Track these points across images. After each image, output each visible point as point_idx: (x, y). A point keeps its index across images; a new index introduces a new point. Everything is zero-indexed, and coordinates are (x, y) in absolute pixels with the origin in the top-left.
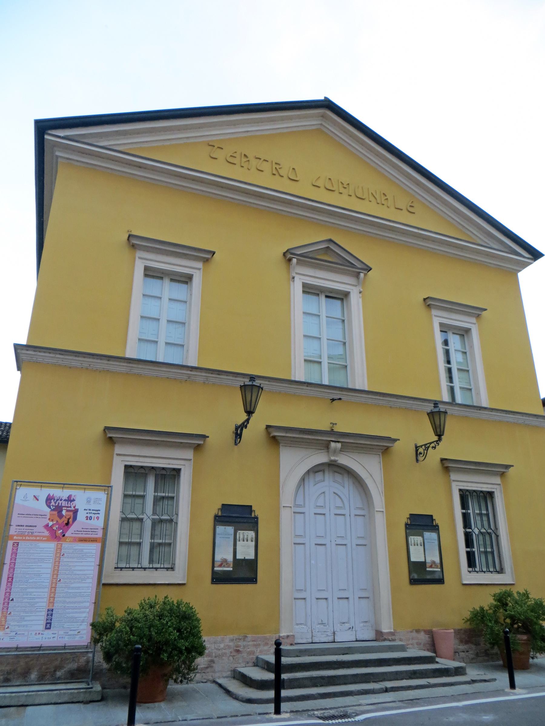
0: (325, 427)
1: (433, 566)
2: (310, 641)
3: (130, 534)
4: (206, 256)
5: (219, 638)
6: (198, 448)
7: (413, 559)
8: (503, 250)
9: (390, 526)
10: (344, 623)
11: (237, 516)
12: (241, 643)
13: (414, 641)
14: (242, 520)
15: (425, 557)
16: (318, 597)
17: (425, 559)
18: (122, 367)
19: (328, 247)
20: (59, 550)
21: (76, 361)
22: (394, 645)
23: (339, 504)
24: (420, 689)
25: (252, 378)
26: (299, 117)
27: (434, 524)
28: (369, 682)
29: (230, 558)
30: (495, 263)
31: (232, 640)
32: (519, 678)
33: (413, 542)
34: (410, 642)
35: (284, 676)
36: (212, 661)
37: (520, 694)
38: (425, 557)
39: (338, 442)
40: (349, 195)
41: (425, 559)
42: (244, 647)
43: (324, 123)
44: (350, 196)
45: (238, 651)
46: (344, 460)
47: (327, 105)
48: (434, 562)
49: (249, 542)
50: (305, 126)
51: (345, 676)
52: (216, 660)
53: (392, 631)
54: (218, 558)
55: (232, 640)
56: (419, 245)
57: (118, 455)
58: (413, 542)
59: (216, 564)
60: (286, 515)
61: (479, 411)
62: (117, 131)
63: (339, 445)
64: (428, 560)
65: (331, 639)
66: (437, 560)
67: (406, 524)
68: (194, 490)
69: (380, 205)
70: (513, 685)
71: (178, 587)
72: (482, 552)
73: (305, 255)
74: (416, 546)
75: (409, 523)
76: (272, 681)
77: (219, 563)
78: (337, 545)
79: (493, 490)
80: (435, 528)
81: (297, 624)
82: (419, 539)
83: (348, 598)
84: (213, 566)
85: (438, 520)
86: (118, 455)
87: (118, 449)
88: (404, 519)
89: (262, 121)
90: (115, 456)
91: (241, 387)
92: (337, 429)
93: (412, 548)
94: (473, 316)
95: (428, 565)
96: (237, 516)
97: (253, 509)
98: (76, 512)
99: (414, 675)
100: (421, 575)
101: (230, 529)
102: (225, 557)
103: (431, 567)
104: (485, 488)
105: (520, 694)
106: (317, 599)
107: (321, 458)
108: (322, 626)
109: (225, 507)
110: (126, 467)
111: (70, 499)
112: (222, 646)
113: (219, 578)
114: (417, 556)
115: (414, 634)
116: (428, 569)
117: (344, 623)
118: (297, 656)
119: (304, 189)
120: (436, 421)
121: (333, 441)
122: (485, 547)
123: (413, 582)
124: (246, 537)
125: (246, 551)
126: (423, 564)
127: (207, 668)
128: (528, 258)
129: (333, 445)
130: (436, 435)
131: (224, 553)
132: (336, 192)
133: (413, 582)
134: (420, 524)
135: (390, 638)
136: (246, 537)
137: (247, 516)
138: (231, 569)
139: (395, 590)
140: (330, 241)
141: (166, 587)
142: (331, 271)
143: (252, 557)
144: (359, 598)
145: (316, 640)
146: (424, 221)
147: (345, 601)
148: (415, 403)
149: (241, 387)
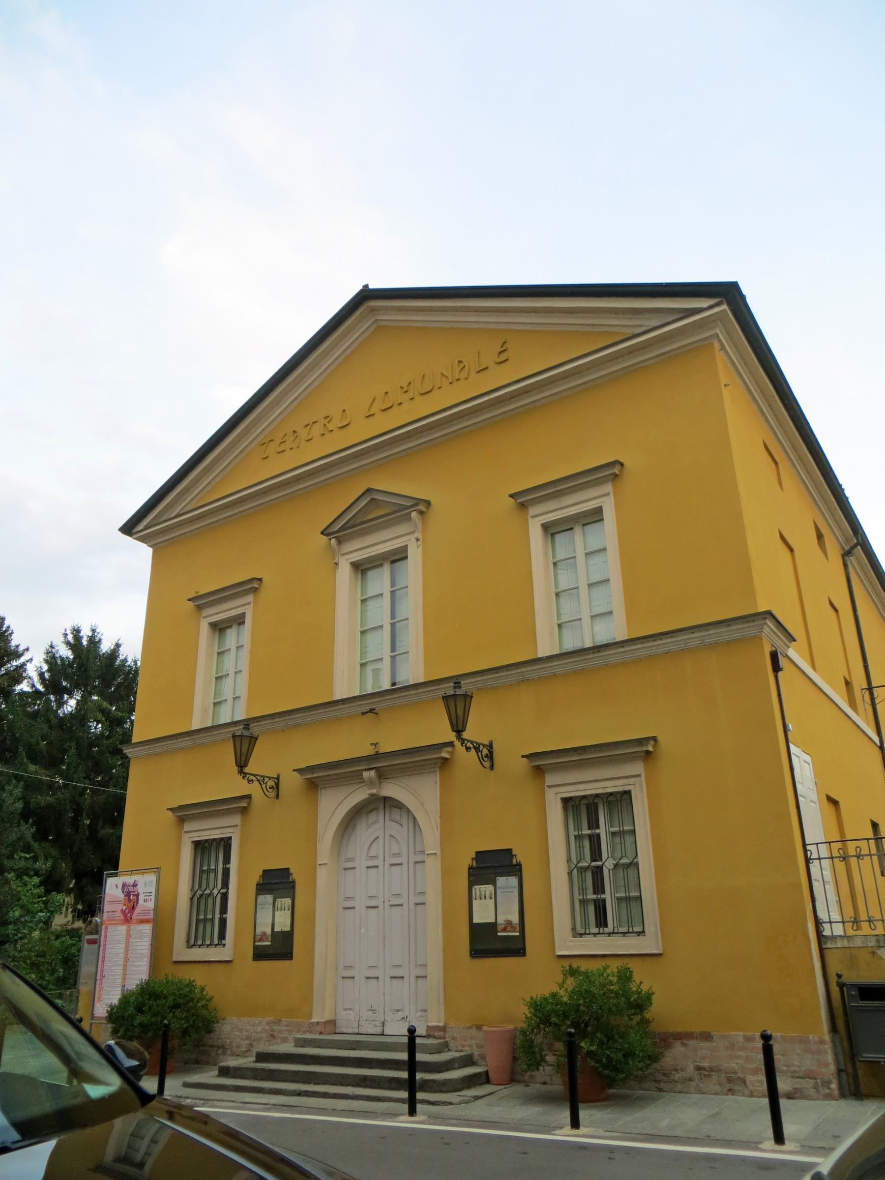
0: (368, 751)
1: (509, 929)
2: (356, 1031)
3: (627, 887)
4: (611, 472)
5: (257, 1021)
6: (244, 811)
7: (475, 921)
8: (669, 320)
9: (446, 873)
10: (398, 1011)
11: (277, 882)
12: (276, 1028)
13: (473, 1041)
14: (282, 886)
15: (496, 915)
16: (369, 975)
17: (496, 919)
18: (570, 664)
19: (372, 499)
20: (128, 931)
21: (174, 744)
22: (386, 1043)
23: (395, 850)
24: (308, 1096)
25: (456, 681)
26: (344, 335)
27: (514, 862)
28: (309, 1083)
29: (269, 931)
30: (652, 355)
31: (268, 1023)
32: (584, 1114)
33: (478, 894)
34: (467, 1043)
35: (404, 1075)
36: (251, 1045)
37: (418, 1123)
38: (496, 915)
39: (372, 769)
40: (411, 399)
41: (496, 919)
42: (279, 1032)
43: (378, 318)
44: (323, 435)
45: (273, 1036)
46: (390, 790)
47: (366, 295)
48: (509, 923)
49: (488, 899)
50: (356, 339)
51: (286, 1072)
52: (254, 1043)
53: (441, 1024)
54: (258, 932)
55: (268, 1023)
56: (512, 410)
57: (549, 787)
58: (478, 894)
59: (258, 938)
60: (322, 876)
61: (599, 654)
62: (178, 494)
63: (373, 773)
64: (501, 920)
65: (379, 1030)
66: (515, 919)
67: (470, 868)
68: (241, 859)
69: (455, 383)
70: (575, 1123)
71: (206, 966)
72: (201, 920)
73: (349, 525)
74: (483, 900)
75: (475, 865)
76: (405, 1079)
77: (503, 927)
78: (391, 906)
79: (627, 788)
80: (515, 870)
81: (345, 1010)
82: (489, 888)
83: (378, 978)
84: (255, 942)
85: (521, 855)
86: (549, 787)
87: (550, 779)
88: (466, 859)
89: (302, 377)
90: (546, 788)
91: (443, 698)
92: (383, 749)
93: (476, 903)
94: (605, 482)
95: (499, 928)
96: (277, 882)
97: (514, 853)
98: (137, 895)
99: (364, 1082)
100: (487, 943)
101: (269, 898)
102: (510, 918)
103: (504, 930)
104: (610, 787)
105: (418, 1123)
106: (368, 978)
107: (360, 795)
108: (371, 1013)
109: (480, 855)
110: (193, 842)
111: (135, 885)
112: (259, 1029)
113: (260, 954)
114: (483, 914)
115: (474, 1032)
116: (499, 934)
117: (398, 1011)
118: (302, 1046)
119: (362, 431)
120: (458, 710)
121: (366, 770)
122: (206, 914)
123: (477, 952)
124: (483, 893)
125: (283, 922)
126: (492, 927)
127: (247, 1051)
128: (711, 307)
129: (366, 774)
130: (453, 731)
131: (264, 927)
132: (396, 406)
133: (477, 952)
134: (492, 865)
135: (436, 1034)
136: (483, 893)
137: (284, 881)
138: (518, 934)
139: (449, 966)
140: (369, 490)
141: (218, 965)
142: (382, 528)
143: (288, 929)
144: (391, 978)
145: (362, 1031)
146: (529, 363)
147: (374, 981)
148: (485, 677)
149: (443, 698)
